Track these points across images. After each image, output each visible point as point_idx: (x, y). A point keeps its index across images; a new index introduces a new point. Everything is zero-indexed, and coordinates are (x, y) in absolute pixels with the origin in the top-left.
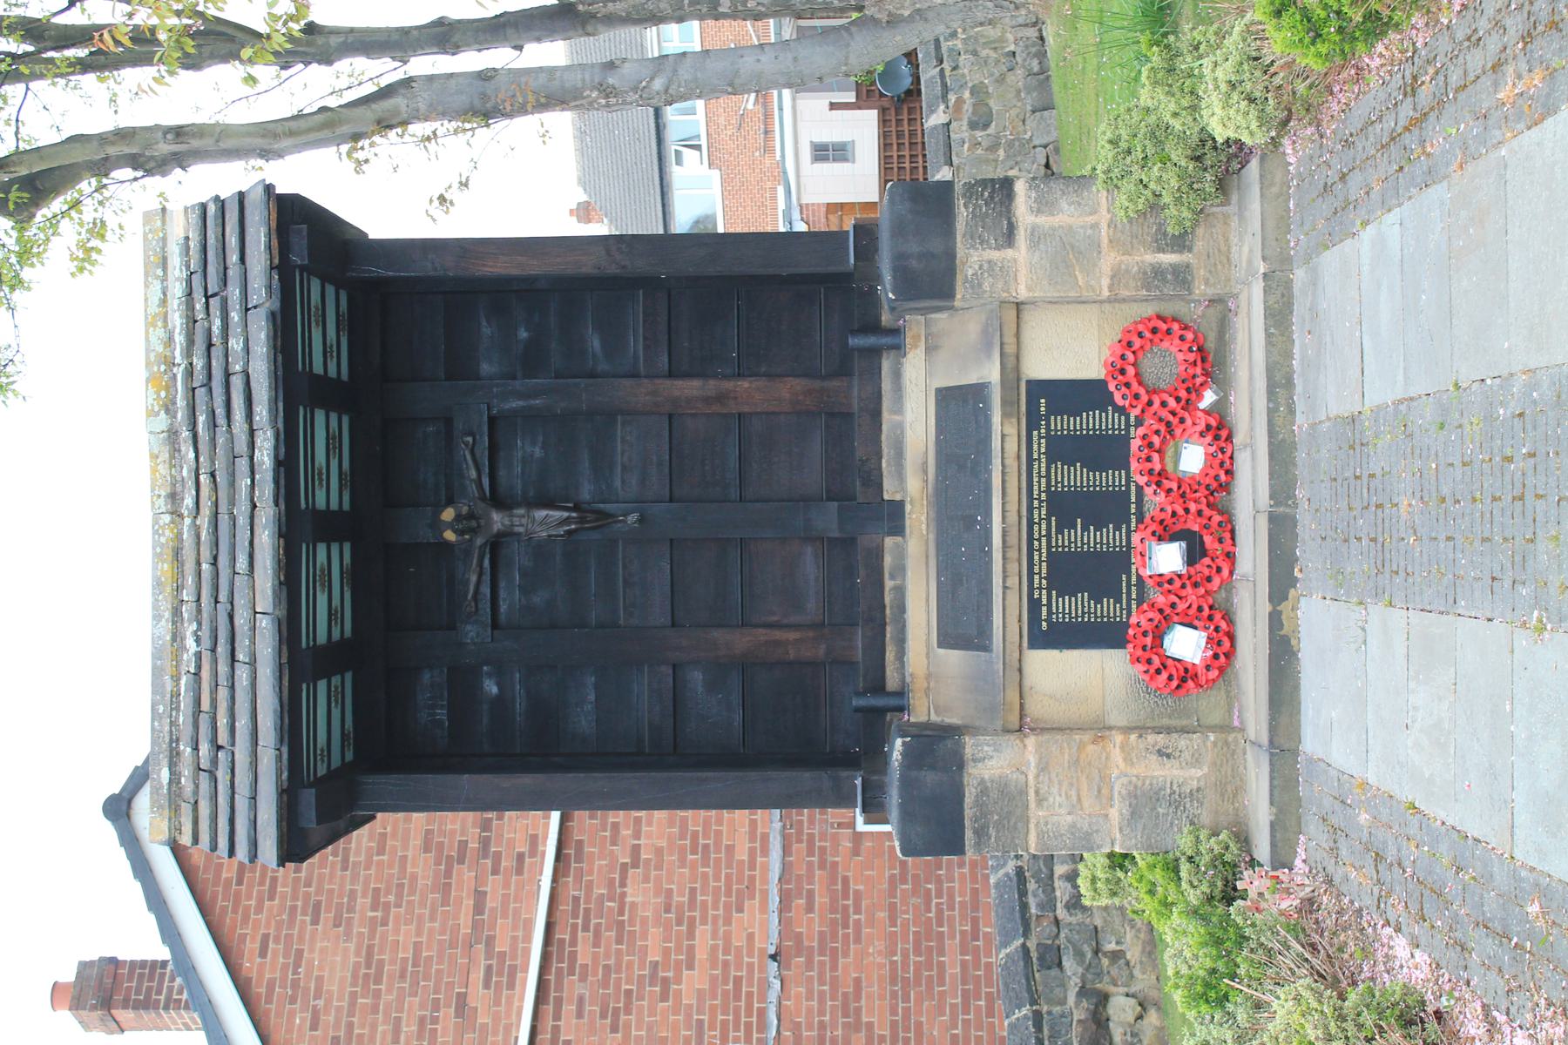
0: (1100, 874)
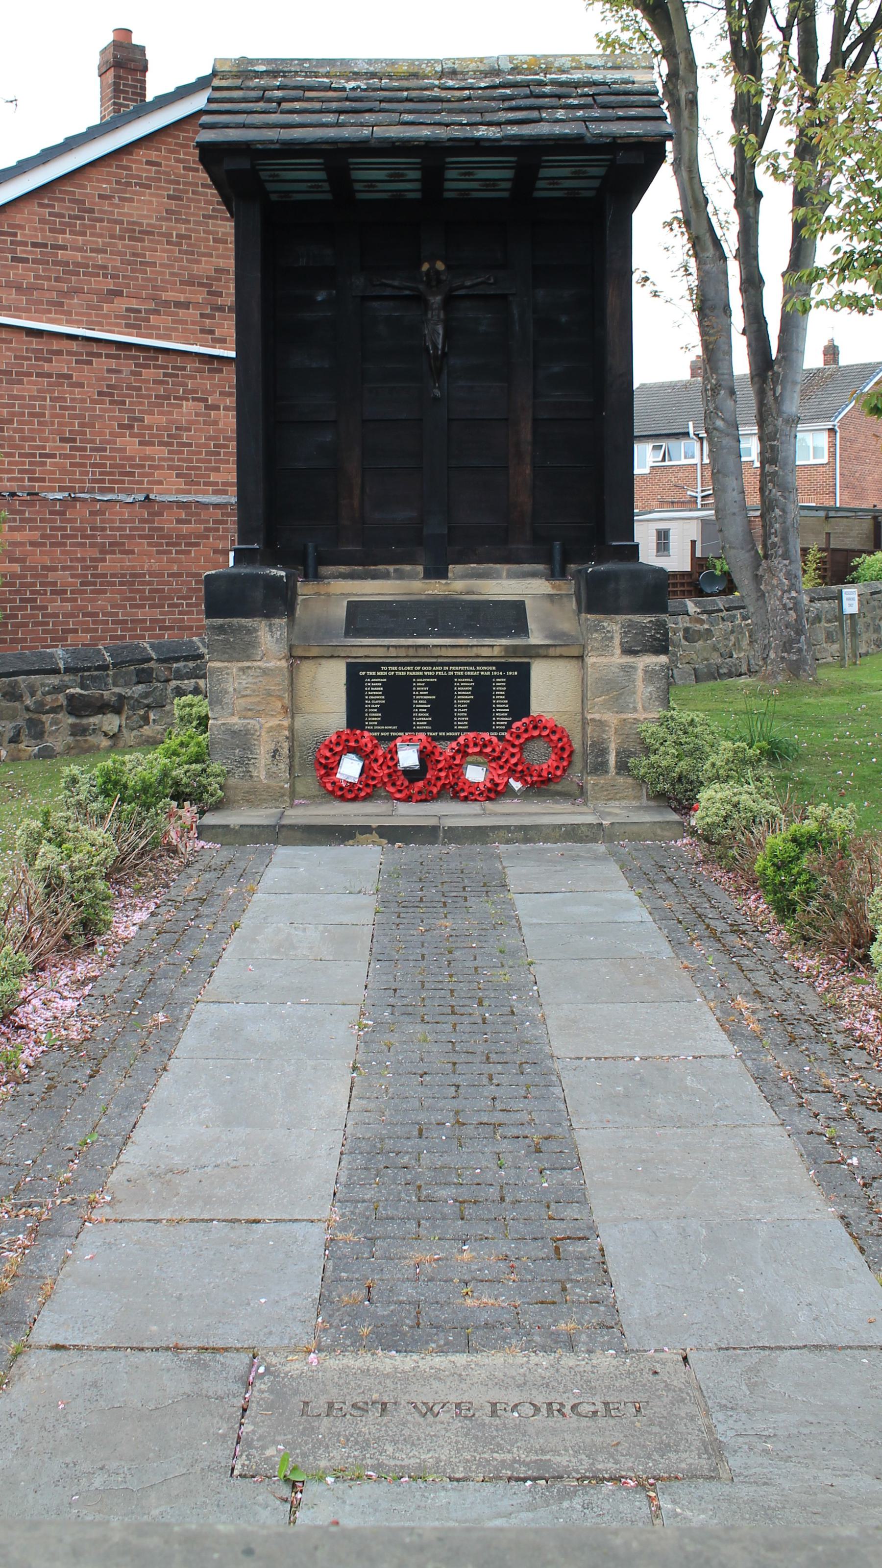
0: (195, 709)
